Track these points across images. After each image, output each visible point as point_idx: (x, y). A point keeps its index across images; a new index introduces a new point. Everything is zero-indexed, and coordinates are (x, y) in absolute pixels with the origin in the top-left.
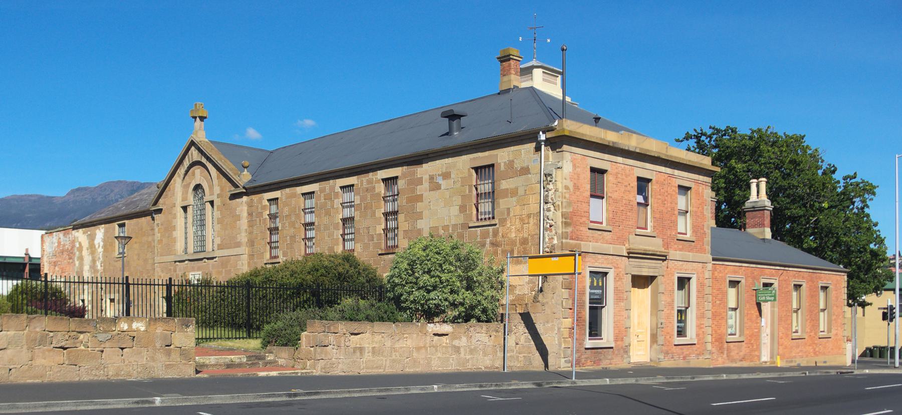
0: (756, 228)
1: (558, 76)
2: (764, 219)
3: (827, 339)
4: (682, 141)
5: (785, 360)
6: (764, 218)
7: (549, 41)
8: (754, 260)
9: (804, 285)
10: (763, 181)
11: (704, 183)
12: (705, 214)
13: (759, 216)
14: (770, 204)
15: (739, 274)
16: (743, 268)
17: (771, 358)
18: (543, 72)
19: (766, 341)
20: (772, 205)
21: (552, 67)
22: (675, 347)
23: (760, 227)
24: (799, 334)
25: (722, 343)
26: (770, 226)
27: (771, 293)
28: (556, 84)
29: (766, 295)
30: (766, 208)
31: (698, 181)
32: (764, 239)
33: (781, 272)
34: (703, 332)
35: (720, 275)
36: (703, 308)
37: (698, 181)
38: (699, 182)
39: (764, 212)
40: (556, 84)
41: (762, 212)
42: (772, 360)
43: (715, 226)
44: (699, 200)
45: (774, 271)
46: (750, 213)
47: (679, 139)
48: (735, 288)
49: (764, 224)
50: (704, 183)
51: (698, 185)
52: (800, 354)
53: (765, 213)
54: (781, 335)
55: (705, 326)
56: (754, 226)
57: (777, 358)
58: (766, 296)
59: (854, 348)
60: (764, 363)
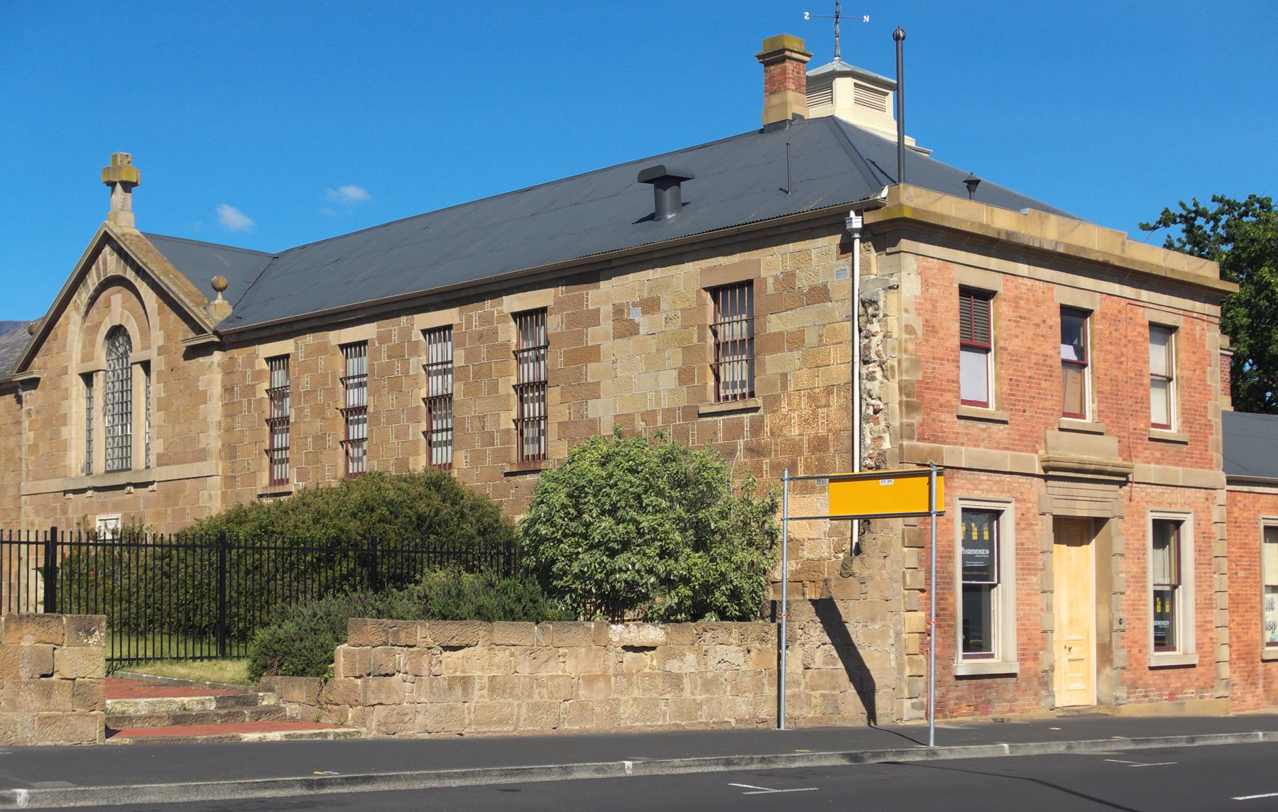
1: (887, 94)
4: (1154, 228)
7: (867, 19)
11: (1205, 317)
18: (856, 85)
21: (874, 75)
28: (883, 109)
35: (1245, 515)
36: (1210, 586)
38: (1195, 315)
40: (883, 109)
43: (1232, 409)
50: (1205, 317)
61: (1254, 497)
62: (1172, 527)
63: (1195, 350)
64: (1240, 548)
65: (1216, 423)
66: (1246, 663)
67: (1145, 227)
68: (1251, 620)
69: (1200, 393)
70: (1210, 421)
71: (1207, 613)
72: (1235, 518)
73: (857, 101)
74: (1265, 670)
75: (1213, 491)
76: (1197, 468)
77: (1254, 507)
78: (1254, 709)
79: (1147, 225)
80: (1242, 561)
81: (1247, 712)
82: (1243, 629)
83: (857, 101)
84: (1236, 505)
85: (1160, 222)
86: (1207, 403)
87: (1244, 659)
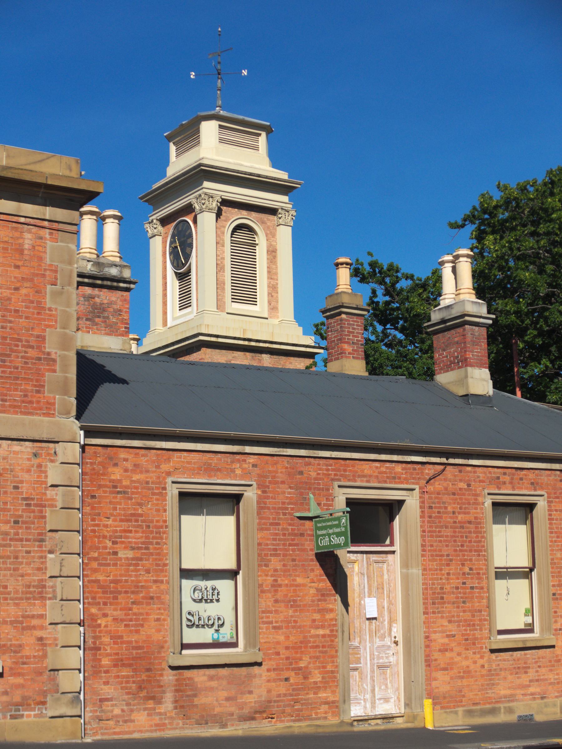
0: (452, 370)
1: (260, 135)
2: (465, 347)
3: (244, 670)
4: (463, 226)
5: (460, 710)
6: (465, 343)
7: (245, 73)
8: (232, 433)
9: (542, 504)
10: (463, 256)
11: (46, 224)
12: (49, 303)
13: (456, 339)
14: (483, 310)
15: (235, 477)
16: (252, 460)
17: (407, 705)
18: (220, 126)
19: (392, 659)
20: (489, 312)
21: (241, 117)
22: (494, 656)
23: (459, 368)
24: (536, 635)
25: (148, 670)
26: (486, 360)
27: (338, 526)
28: (256, 148)
29: (331, 531)
30: (467, 318)
31: (15, 219)
32: (466, 395)
33: (429, 471)
34: (41, 639)
35: (136, 477)
36: (39, 569)
37: (15, 219)
38: (22, 220)
39: (464, 330)
40: (256, 148)
41: (460, 330)
42: (408, 710)
43: (367, 374)
44: (17, 267)
45: (399, 468)
46: (440, 335)
47: (456, 223)
48: (233, 515)
49: (466, 359)
50: (46, 224)
51: (16, 229)
52: (532, 690)
53: (469, 336)
54: (440, 639)
55: (48, 621)
56: (448, 368)
57: (422, 706)
58: (329, 535)
59: (346, 699)
60: (355, 723)
61: (158, 455)
62: (383, 514)
63: (20, 263)
64: (122, 520)
65: (63, 358)
66: (135, 670)
67: (454, 226)
68: (147, 614)
69: (27, 318)
70: (49, 354)
71: (30, 604)
72: (113, 481)
73: (221, 141)
74: (177, 680)
75: (51, 445)
76: (16, 413)
77: (158, 467)
78: (151, 731)
79: (456, 223)
80: (127, 537)
81: (136, 736)
82: (126, 626)
83: (221, 141)
84: (116, 465)
85: (465, 220)
86: (44, 331)
87: (130, 665)
